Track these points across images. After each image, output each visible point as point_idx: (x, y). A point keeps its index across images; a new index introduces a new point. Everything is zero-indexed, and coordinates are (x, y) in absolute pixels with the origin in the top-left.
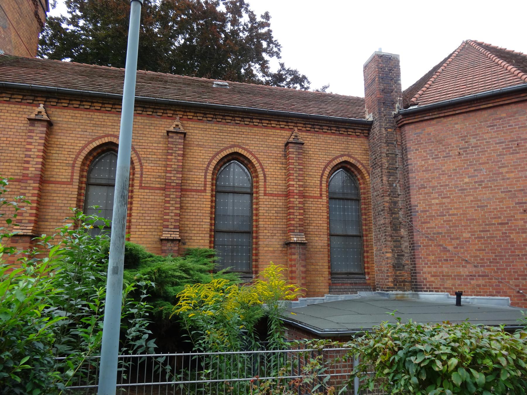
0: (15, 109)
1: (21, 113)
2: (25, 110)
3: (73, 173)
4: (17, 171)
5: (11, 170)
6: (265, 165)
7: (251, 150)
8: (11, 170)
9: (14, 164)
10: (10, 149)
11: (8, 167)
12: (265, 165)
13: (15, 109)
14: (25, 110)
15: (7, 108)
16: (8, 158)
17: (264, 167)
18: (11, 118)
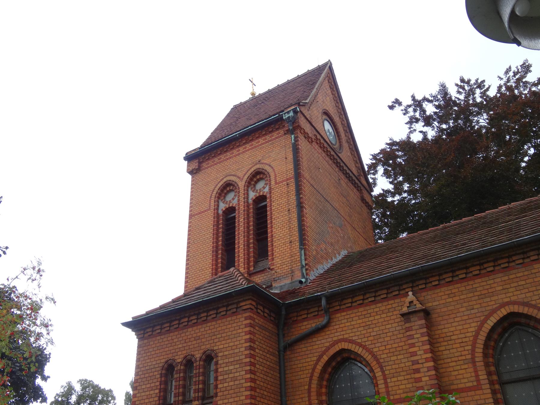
0: (383, 308)
1: (391, 310)
2: (394, 306)
3: (387, 387)
4: (408, 386)
5: (401, 387)
6: (383, 356)
7: (359, 341)
8: (401, 387)
9: (402, 378)
10: (393, 358)
11: (397, 383)
12: (383, 356)
13: (383, 308)
14: (394, 306)
15: (376, 310)
16: (394, 371)
17: (381, 361)
18: (382, 320)
